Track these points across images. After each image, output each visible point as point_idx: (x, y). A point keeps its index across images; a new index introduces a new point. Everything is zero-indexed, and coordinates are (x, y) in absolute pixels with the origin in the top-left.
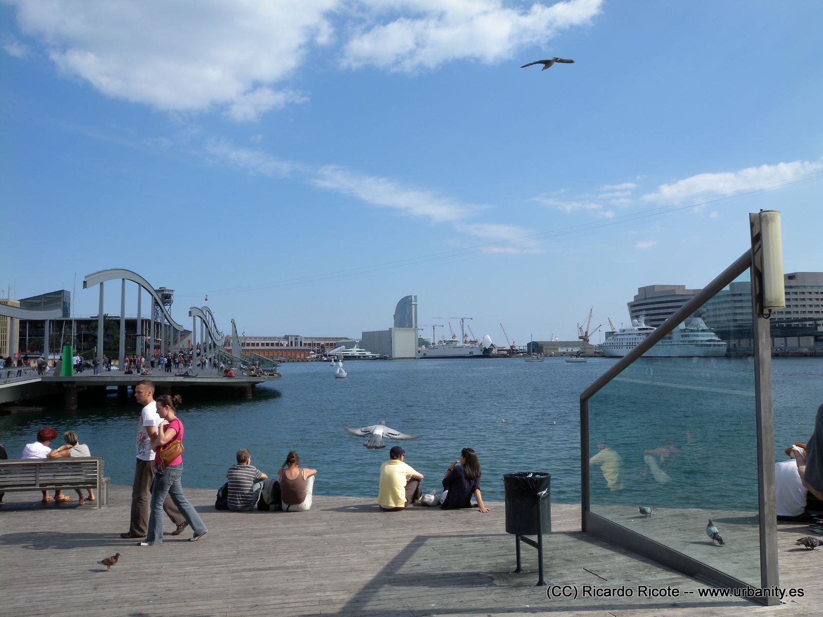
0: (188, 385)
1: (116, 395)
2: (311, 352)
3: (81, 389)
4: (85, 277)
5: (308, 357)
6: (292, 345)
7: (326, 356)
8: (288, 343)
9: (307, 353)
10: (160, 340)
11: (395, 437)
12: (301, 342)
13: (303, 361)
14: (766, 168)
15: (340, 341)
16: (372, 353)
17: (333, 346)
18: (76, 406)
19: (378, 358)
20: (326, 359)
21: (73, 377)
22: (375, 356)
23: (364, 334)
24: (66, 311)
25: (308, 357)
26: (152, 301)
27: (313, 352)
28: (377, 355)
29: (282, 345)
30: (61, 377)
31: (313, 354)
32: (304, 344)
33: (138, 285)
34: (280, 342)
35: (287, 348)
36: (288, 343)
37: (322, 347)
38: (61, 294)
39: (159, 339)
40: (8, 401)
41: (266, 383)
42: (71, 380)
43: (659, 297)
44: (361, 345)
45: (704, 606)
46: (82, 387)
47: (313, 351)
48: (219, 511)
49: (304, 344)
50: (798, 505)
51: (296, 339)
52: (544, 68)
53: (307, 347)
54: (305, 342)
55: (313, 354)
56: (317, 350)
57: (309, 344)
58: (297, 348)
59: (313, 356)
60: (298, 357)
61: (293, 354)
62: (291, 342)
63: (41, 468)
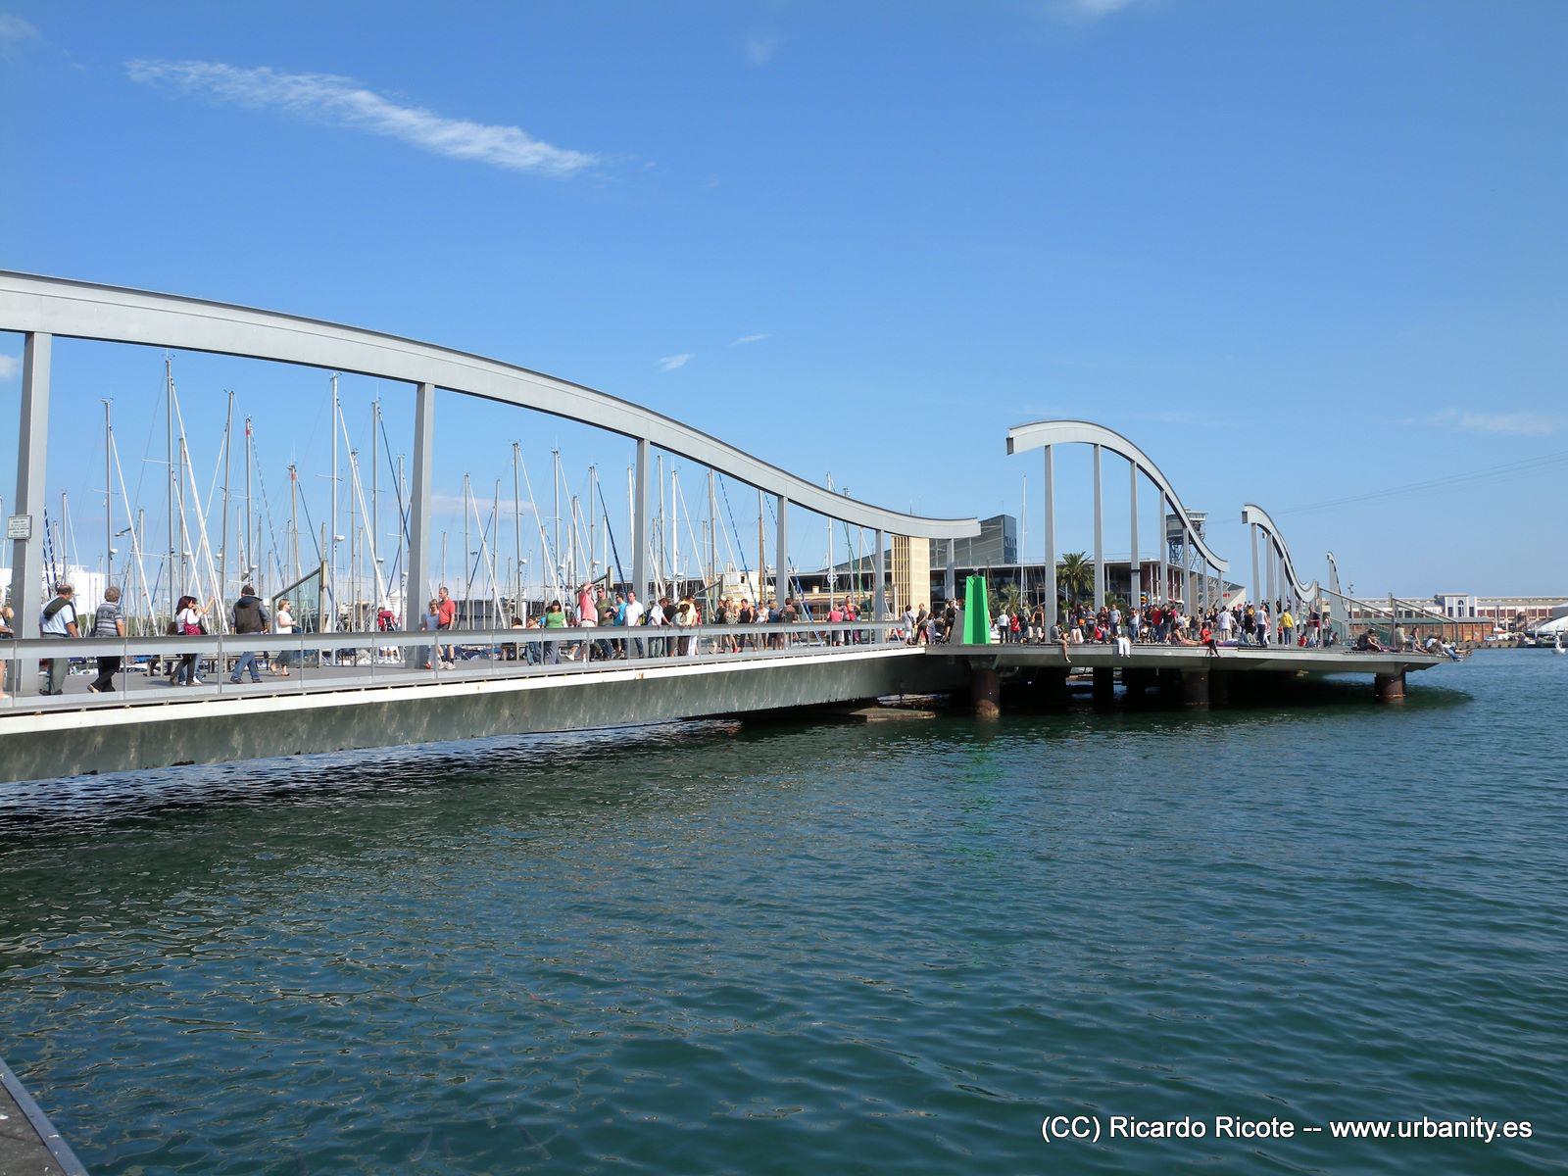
2: (1497, 629)
3: (1009, 674)
5: (1491, 639)
6: (1451, 614)
7: (1532, 636)
8: (1444, 611)
9: (1488, 630)
10: (1183, 602)
11: (994, 1099)
12: (1472, 609)
13: (1479, 647)
18: (997, 711)
20: (1533, 642)
21: (988, 646)
24: (1010, 553)
25: (1491, 639)
27: (1500, 629)
30: (966, 646)
36: (1444, 611)
37: (1520, 617)
38: (998, 523)
40: (863, 696)
42: (984, 652)
46: (1011, 669)
47: (1500, 626)
48: (1287, 667)
51: (1460, 602)
53: (1486, 618)
54: (1482, 608)
57: (1491, 613)
58: (1472, 620)
59: (1500, 637)
60: (1468, 638)
61: (1477, 634)
62: (1450, 609)
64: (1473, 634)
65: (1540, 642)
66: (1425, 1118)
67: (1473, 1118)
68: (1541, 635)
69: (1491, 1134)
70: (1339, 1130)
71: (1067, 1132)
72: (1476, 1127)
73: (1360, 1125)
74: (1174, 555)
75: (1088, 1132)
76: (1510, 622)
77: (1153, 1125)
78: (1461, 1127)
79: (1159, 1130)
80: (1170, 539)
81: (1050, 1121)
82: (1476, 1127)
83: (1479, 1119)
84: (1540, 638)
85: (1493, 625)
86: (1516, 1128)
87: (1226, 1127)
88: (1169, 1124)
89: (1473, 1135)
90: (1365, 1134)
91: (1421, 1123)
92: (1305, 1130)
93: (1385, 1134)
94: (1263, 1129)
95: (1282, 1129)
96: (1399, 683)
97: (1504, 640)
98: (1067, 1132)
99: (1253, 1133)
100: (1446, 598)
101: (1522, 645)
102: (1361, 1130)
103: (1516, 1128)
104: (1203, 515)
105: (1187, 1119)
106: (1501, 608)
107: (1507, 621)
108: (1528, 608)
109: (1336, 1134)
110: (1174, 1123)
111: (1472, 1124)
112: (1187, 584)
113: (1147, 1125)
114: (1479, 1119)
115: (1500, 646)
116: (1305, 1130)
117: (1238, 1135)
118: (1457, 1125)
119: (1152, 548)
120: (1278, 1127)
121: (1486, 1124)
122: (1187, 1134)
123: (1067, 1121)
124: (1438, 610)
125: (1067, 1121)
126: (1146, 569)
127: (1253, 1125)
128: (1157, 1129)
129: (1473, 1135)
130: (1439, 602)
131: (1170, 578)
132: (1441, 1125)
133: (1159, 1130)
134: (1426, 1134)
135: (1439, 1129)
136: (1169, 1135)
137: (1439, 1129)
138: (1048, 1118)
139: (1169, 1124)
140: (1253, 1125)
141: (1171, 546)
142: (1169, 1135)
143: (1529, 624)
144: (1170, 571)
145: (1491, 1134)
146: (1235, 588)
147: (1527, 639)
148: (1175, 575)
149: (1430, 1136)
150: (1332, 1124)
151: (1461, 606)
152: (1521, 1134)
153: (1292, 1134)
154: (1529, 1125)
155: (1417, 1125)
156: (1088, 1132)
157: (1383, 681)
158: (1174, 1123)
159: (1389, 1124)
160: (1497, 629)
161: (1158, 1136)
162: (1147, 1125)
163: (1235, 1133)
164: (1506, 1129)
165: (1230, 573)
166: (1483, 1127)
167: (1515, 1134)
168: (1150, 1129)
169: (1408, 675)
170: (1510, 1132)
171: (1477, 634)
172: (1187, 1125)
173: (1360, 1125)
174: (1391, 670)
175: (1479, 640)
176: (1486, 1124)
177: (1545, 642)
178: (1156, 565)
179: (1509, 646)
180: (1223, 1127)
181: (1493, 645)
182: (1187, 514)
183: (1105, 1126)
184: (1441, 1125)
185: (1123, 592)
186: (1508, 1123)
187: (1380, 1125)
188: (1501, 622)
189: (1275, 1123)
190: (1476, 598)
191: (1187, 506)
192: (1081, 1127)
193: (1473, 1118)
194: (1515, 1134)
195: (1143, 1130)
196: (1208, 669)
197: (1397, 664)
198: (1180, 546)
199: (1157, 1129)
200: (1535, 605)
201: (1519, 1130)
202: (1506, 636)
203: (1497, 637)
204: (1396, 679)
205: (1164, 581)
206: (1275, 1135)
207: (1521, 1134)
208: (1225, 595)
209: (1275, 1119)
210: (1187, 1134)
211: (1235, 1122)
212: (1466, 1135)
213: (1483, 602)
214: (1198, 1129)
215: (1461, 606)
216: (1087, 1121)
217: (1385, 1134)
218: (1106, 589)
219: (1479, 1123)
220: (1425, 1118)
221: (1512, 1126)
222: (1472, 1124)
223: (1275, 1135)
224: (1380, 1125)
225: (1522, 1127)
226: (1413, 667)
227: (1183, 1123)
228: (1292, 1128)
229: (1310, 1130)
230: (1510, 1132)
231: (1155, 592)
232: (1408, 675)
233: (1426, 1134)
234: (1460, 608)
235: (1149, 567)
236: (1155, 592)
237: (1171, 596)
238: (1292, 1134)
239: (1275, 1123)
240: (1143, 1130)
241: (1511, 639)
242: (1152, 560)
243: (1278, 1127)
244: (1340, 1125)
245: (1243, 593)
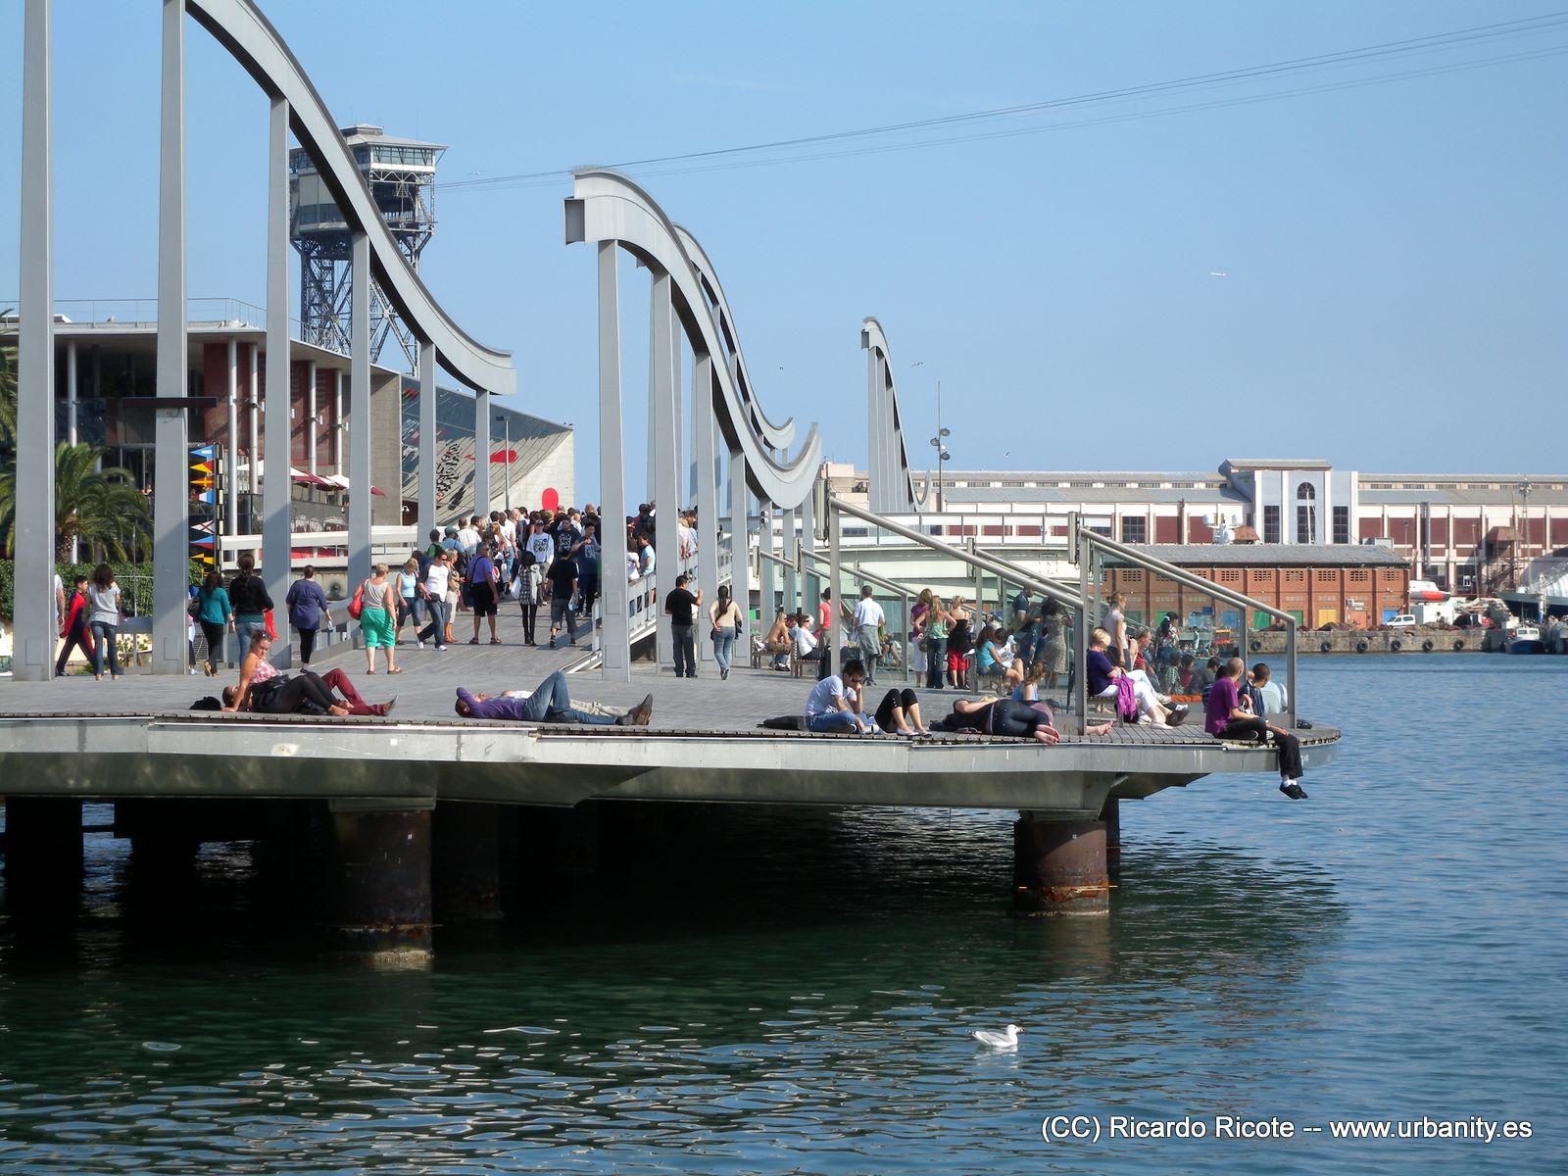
0: (573, 798)
1: (242, 861)
2: (1419, 586)
4: (389, 567)
7: (1525, 609)
8: (1250, 520)
10: (344, 482)
12: (1341, 515)
14: (1198, 544)
20: (1531, 635)
26: (276, 142)
27: (1431, 587)
29: (1202, 531)
31: (1428, 599)
32: (1363, 522)
34: (1192, 510)
35: (1243, 554)
36: (1250, 520)
37: (1493, 546)
39: (339, 479)
41: (1209, 812)
47: (1430, 573)
49: (1363, 522)
51: (1305, 490)
53: (1386, 544)
54: (1373, 512)
55: (1428, 599)
56: (1460, 570)
57: (1401, 529)
58: (1341, 554)
59: (1430, 613)
60: (1326, 616)
61: (1358, 605)
62: (1272, 514)
63: (107, 1070)
64: (1343, 603)
65: (1556, 633)
66: (1425, 1119)
67: (1472, 1118)
69: (1491, 1134)
71: (1067, 1132)
72: (1476, 1127)
73: (1360, 1125)
74: (318, 300)
75: (1088, 1131)
76: (1463, 561)
77: (1153, 1125)
78: (1461, 1127)
79: (1160, 1129)
80: (306, 236)
81: (1050, 1121)
82: (1476, 1127)
83: (1479, 1119)
84: (1554, 621)
85: (1406, 569)
86: (1516, 1128)
87: (1226, 1127)
88: (1169, 1125)
89: (1473, 1135)
90: (1364, 1134)
91: (1421, 1123)
92: (1305, 1130)
94: (1263, 1130)
95: (1282, 1129)
96: (1097, 837)
97: (1442, 625)
98: (1067, 1132)
100: (1258, 474)
101: (1498, 644)
103: (1516, 1128)
104: (426, 153)
105: (1187, 1118)
106: (1437, 512)
107: (1452, 557)
108: (1519, 511)
109: (1336, 1134)
110: (1174, 1123)
111: (1473, 1124)
112: (365, 419)
113: (1147, 1125)
114: (1479, 1119)
115: (1427, 647)
116: (1305, 1130)
117: (1238, 1135)
118: (1457, 1125)
119: (240, 279)
120: (1278, 1127)
121: (1486, 1124)
122: (1187, 1134)
123: (1067, 1121)
124: (1234, 512)
125: (1067, 1121)
126: (213, 356)
127: (1253, 1125)
128: (1156, 1129)
129: (1473, 1135)
130: (1236, 486)
131: (300, 391)
132: (1441, 1125)
134: (1426, 1134)
135: (1439, 1128)
136: (1169, 1135)
138: (1048, 1118)
140: (1253, 1125)
141: (306, 266)
142: (1169, 1135)
143: (1523, 566)
144: (300, 367)
145: (1491, 1134)
146: (521, 430)
147: (1513, 623)
148: (319, 379)
149: (1430, 1136)
150: (1332, 1124)
151: (1308, 503)
152: (1521, 1134)
153: (1291, 1134)
154: (1529, 1125)
155: (1417, 1125)
156: (1088, 1131)
157: (1039, 835)
158: (1174, 1123)
160: (1419, 586)
161: (1158, 1136)
162: (1147, 1125)
163: (1129, 1133)
164: (1506, 1129)
165: (505, 384)
166: (1483, 1126)
167: (1515, 1133)
169: (1127, 809)
171: (1358, 605)
172: (1187, 1125)
173: (1360, 1125)
174: (1072, 799)
175: (1363, 625)
176: (1486, 1124)
178: (249, 347)
179: (1459, 646)
180: (1223, 1127)
181: (1411, 644)
182: (360, 154)
183: (1105, 1127)
184: (1441, 1125)
185: (125, 438)
186: (1508, 1124)
187: (1380, 1125)
188: (1435, 560)
189: (1275, 1123)
190: (1355, 475)
191: (368, 99)
193: (1472, 1118)
194: (1515, 1133)
196: (429, 803)
197: (1091, 780)
198: (340, 266)
199: (1156, 1129)
200: (1538, 503)
201: (1519, 1130)
202: (1449, 610)
203: (1420, 615)
204: (1082, 827)
205: (278, 404)
206: (1275, 1135)
207: (1521, 1134)
208: (498, 458)
209: (1275, 1119)
210: (1187, 1134)
211: (1235, 1121)
212: (1466, 1135)
213: (1378, 489)
214: (1198, 1130)
215: (1308, 503)
216: (1087, 1121)
218: (62, 433)
220: (1425, 1119)
221: (1512, 1126)
222: (1473, 1124)
223: (1275, 1135)
224: (1380, 1125)
225: (1522, 1127)
226: (1138, 786)
227: (1183, 1123)
228: (1292, 1128)
229: (1310, 1130)
231: (245, 445)
232: (1127, 809)
233: (1426, 1134)
234: (1302, 510)
235: (118, 454)
236: (245, 445)
237: (302, 459)
238: (1291, 1134)
239: (1275, 1123)
240: (1143, 1129)
241: (1463, 622)
242: (235, 326)
243: (1278, 1127)
245: (563, 450)
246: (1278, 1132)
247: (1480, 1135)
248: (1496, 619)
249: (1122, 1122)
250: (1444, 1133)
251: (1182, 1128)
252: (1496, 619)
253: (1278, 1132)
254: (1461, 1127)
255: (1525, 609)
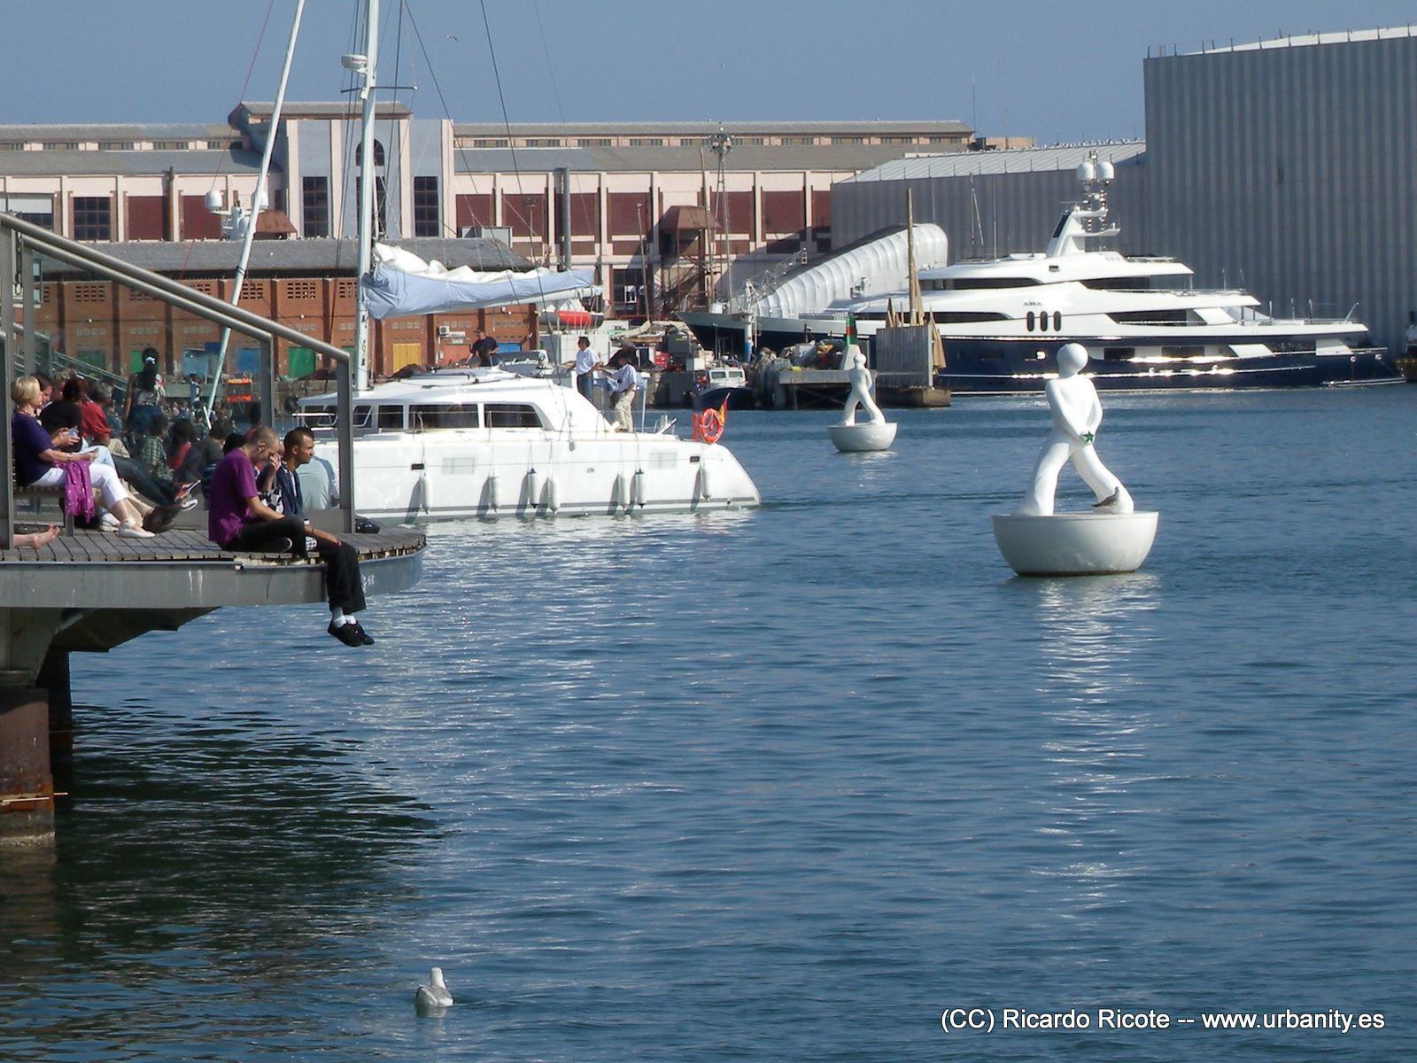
6: (316, 219)
7: (725, 339)
12: (427, 190)
15: (891, 171)
16: (1275, 302)
17: (817, 233)
19: (1336, 368)
20: (733, 379)
22: (1310, 341)
23: (1171, 82)
28: (1334, 335)
33: (163, 303)
34: (186, 186)
43: (1165, 429)
44: (1142, 213)
45: (381, 349)
50: (34, 371)
52: (861, 287)
54: (480, 185)
62: (315, 189)
66: (1288, 1011)
68: (777, 339)
69: (1347, 1025)
70: (1210, 1021)
71: (964, 1023)
72: (1334, 1018)
73: (1229, 1017)
75: (983, 1023)
77: (1042, 1017)
78: (1321, 1019)
81: (949, 1014)
82: (1334, 1018)
88: (1057, 1016)
93: (1251, 1025)
95: (1158, 1020)
98: (964, 1023)
99: (1132, 1024)
102: (1229, 1021)
103: (1370, 1020)
106: (580, 184)
109: (1207, 1025)
113: (1037, 1017)
118: (1317, 1016)
120: (1155, 1019)
121: (1343, 1016)
122: (1072, 1025)
123: (964, 1014)
125: (964, 1014)
127: (1132, 1017)
132: (1302, 1017)
133: (1048, 1022)
134: (1289, 1025)
135: (1300, 1020)
137: (1300, 1020)
139: (1057, 1016)
145: (1347, 1025)
150: (1204, 1016)
154: (1382, 1017)
156: (983, 1023)
159: (1255, 1016)
162: (1037, 1017)
163: (1020, 1024)
164: (1361, 1020)
166: (1340, 1019)
168: (1039, 1020)
170: (1365, 1023)
173: (1229, 1017)
177: (796, 375)
187: (1247, 1017)
189: (1152, 1015)
192: (977, 1019)
195: (1033, 1021)
201: (1373, 1021)
207: (1375, 1025)
210: (1072, 1025)
211: (1116, 1014)
214: (1083, 1021)
216: (982, 1013)
217: (1251, 1025)
219: (1337, 1015)
220: (1288, 1011)
223: (1153, 1026)
224: (1247, 1017)
225: (1375, 1019)
228: (1168, 1020)
230: (1365, 1023)
238: (1167, 1025)
239: (1152, 1015)
243: (1155, 1019)
244: (1211, 1017)
246: (1155, 1023)
247: (1337, 1026)
248: (677, 355)
249: (1014, 1014)
250: (1305, 1024)
251: (1069, 1021)
252: (677, 355)
253: (1155, 1023)
254: (1321, 1019)
255: (725, 339)
